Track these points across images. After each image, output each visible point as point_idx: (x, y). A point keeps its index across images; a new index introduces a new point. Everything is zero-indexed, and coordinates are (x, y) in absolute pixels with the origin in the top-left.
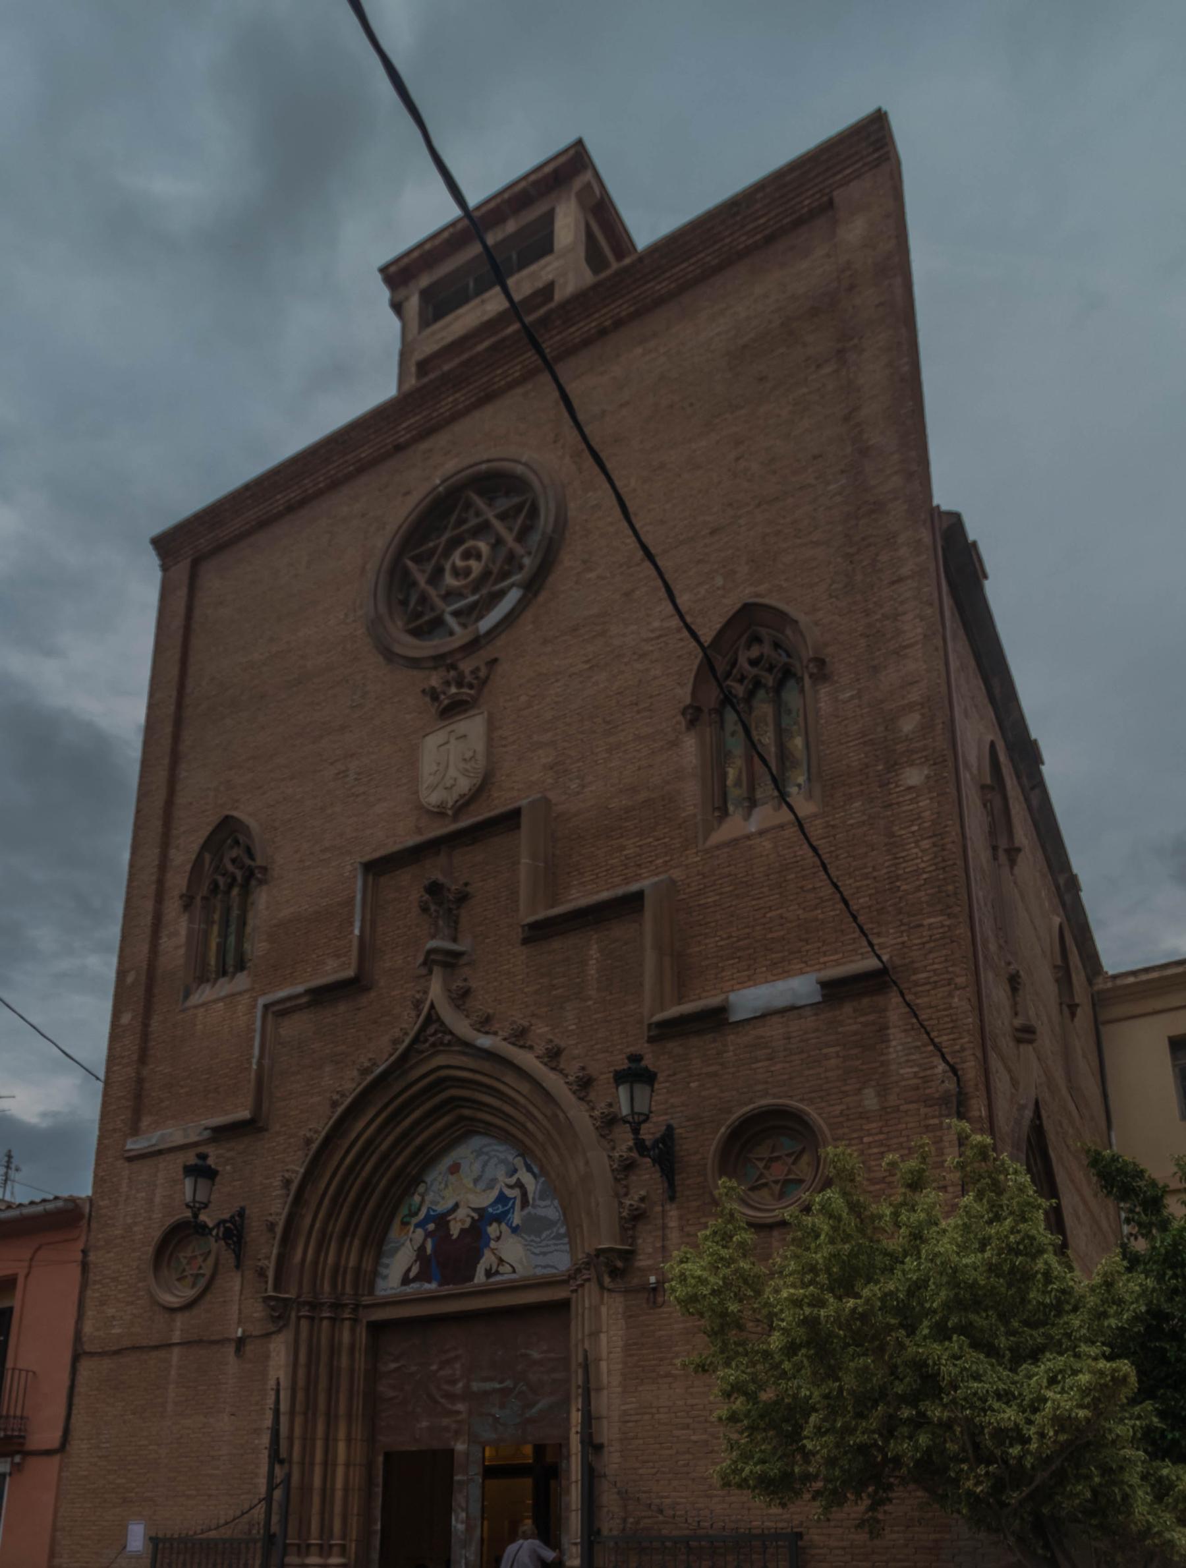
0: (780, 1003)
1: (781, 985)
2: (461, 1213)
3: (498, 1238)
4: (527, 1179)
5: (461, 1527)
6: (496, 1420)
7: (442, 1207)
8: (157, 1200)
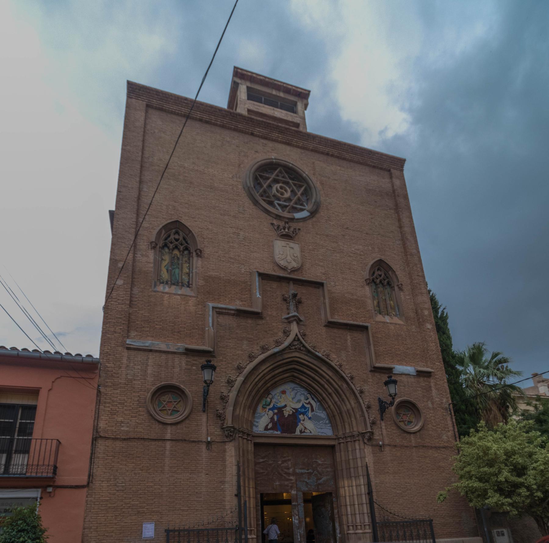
0: (406, 372)
1: (405, 368)
2: (288, 409)
3: (304, 420)
4: (313, 402)
5: (296, 521)
6: (307, 483)
7: (279, 405)
8: (149, 372)
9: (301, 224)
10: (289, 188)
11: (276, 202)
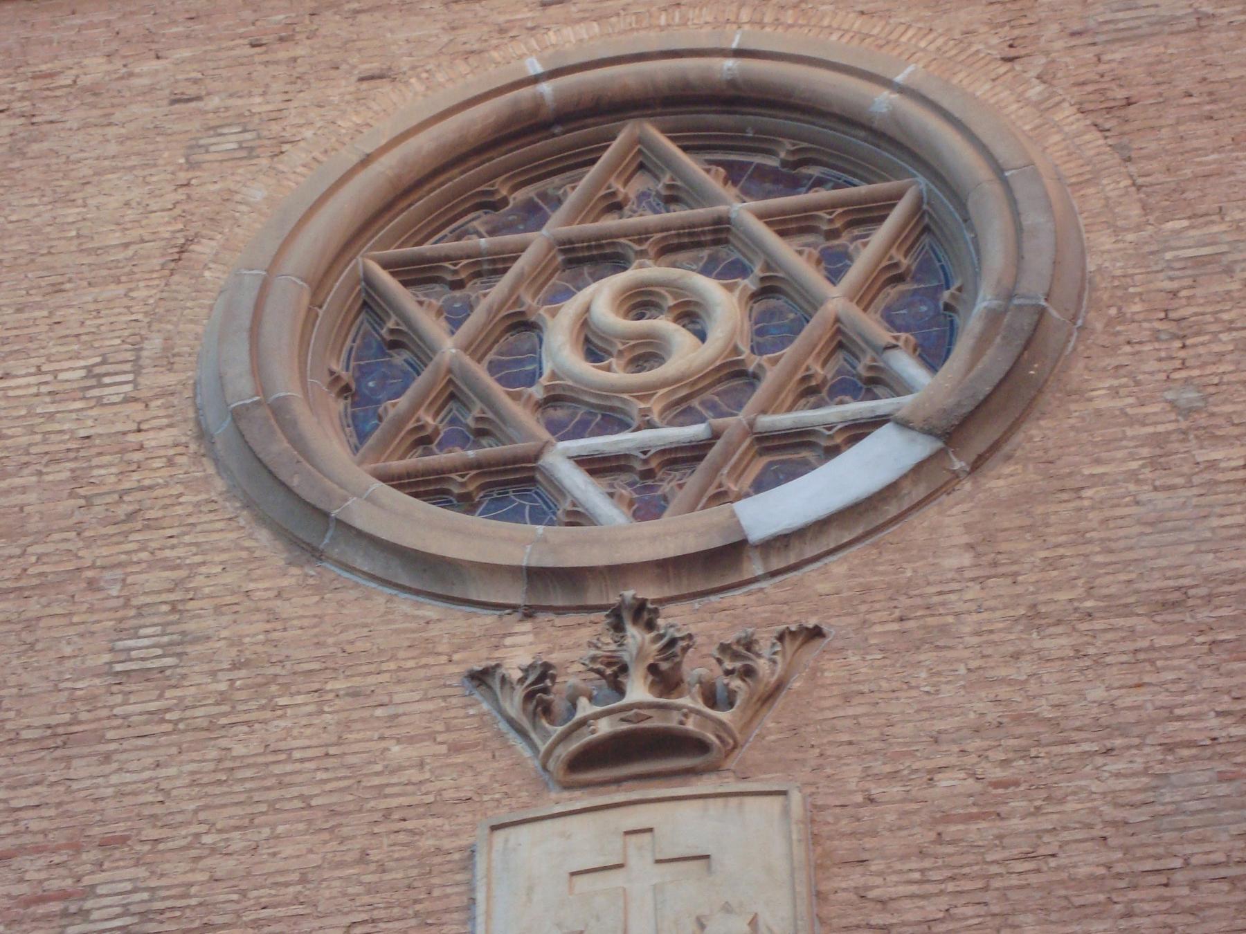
9: (827, 582)
10: (730, 272)
11: (560, 461)
